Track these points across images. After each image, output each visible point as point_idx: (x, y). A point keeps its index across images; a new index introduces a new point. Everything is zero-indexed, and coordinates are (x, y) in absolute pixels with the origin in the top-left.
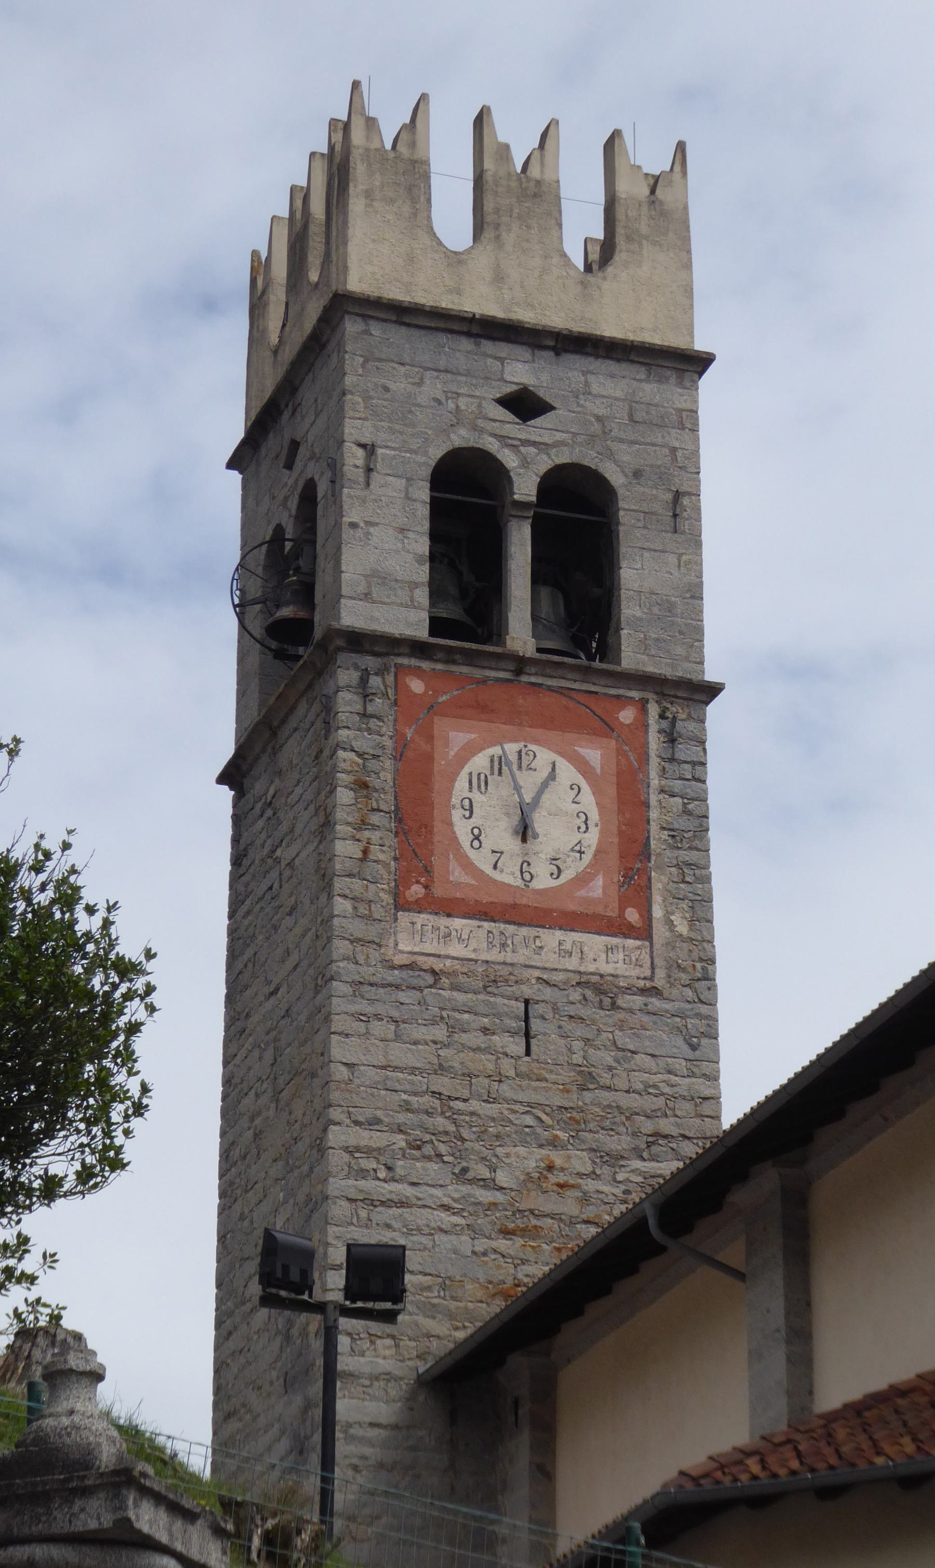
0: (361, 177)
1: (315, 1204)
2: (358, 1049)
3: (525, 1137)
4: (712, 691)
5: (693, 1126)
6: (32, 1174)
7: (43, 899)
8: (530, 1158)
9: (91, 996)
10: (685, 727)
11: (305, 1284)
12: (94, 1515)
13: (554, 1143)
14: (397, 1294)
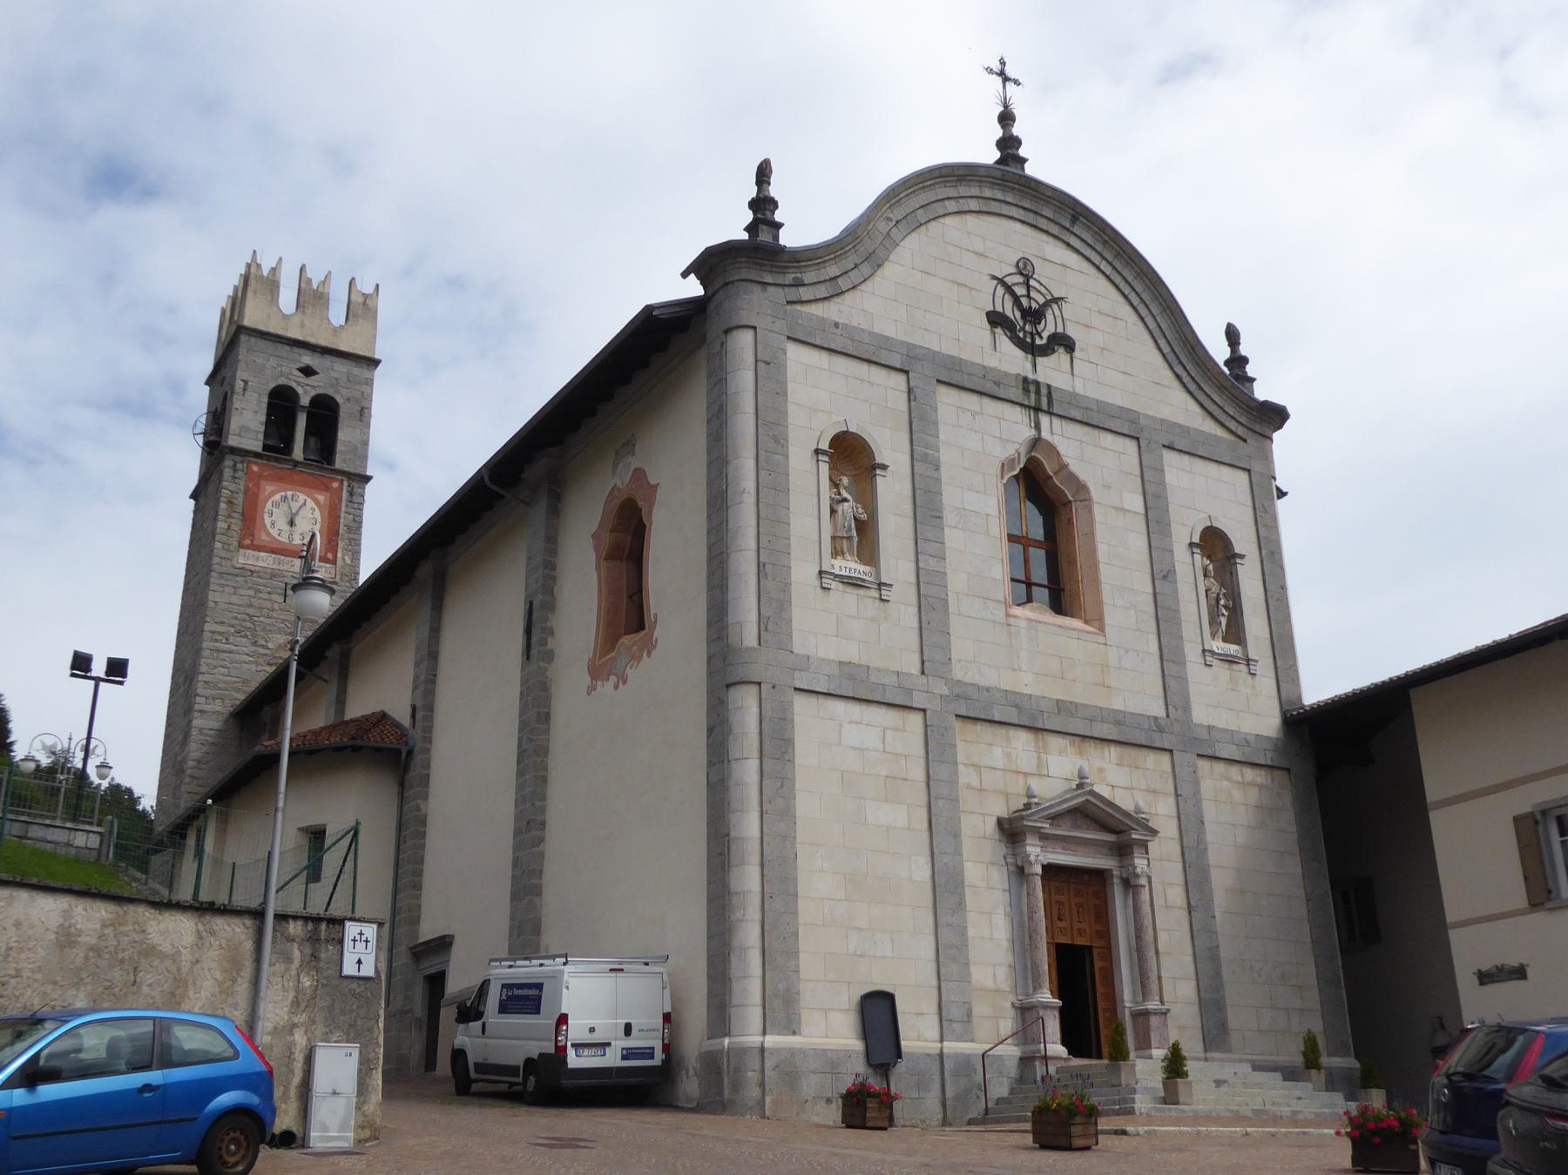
0: (252, 282)
2: (217, 596)
4: (368, 479)
10: (357, 490)
14: (124, 675)
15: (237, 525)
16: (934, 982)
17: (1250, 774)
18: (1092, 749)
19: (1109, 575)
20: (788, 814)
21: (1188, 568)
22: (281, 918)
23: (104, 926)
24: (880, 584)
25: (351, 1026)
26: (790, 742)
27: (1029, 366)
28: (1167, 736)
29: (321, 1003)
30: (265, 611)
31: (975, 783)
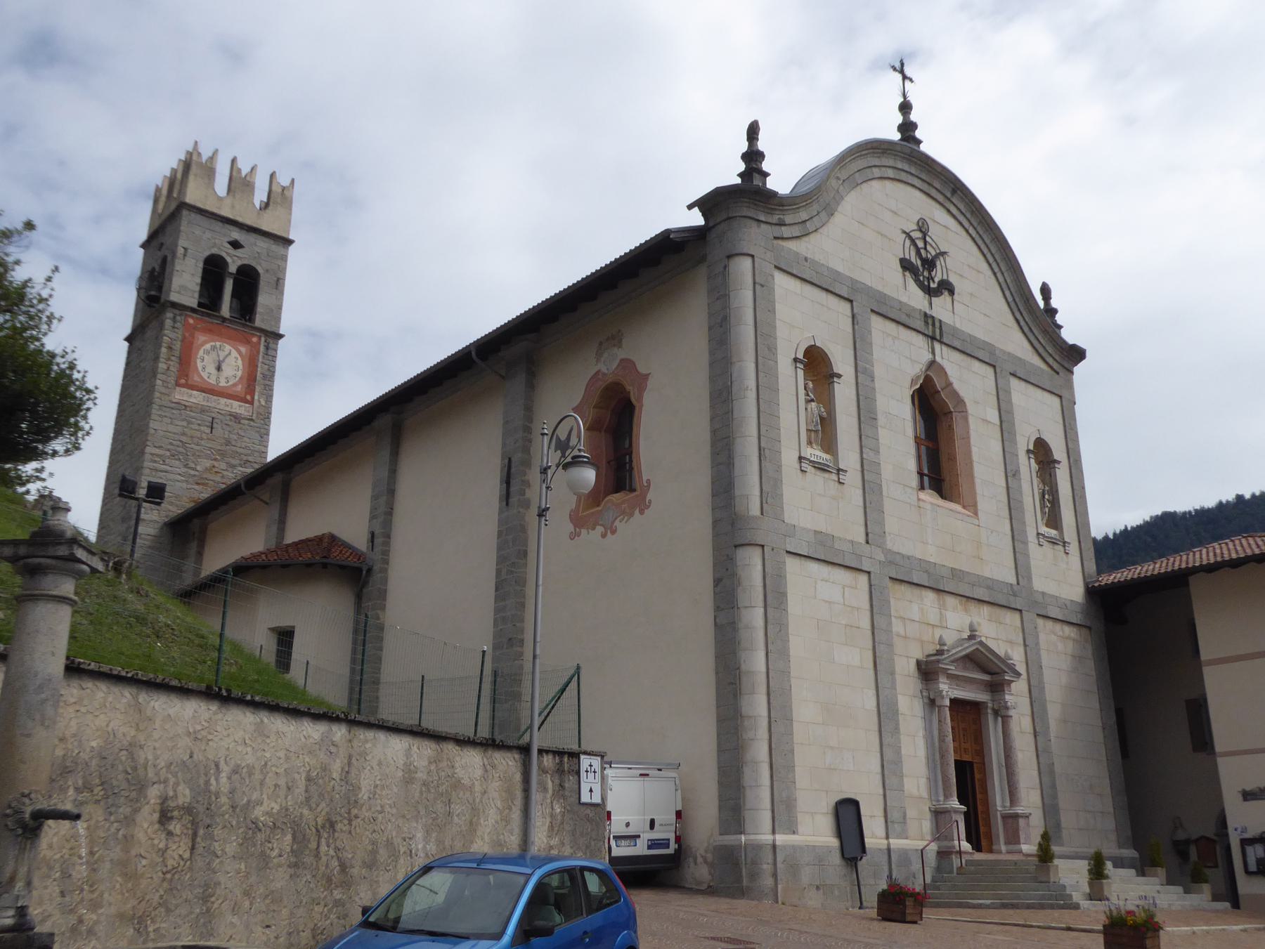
0: (194, 169)
1: (138, 469)
2: (158, 425)
3: (208, 457)
4: (281, 336)
5: (258, 460)
6: (49, 449)
7: (63, 366)
8: (208, 463)
9: (75, 398)
11: (134, 492)
12: (62, 551)
13: (215, 460)
14: (162, 497)
15: (174, 366)
16: (881, 791)
17: (1068, 630)
18: (973, 607)
19: (979, 471)
20: (785, 653)
21: (1027, 467)
22: (540, 751)
23: (430, 763)
24: (839, 470)
25: (587, 847)
26: (784, 594)
27: (926, 303)
28: (1009, 599)
29: (567, 828)
30: (196, 440)
31: (902, 633)
